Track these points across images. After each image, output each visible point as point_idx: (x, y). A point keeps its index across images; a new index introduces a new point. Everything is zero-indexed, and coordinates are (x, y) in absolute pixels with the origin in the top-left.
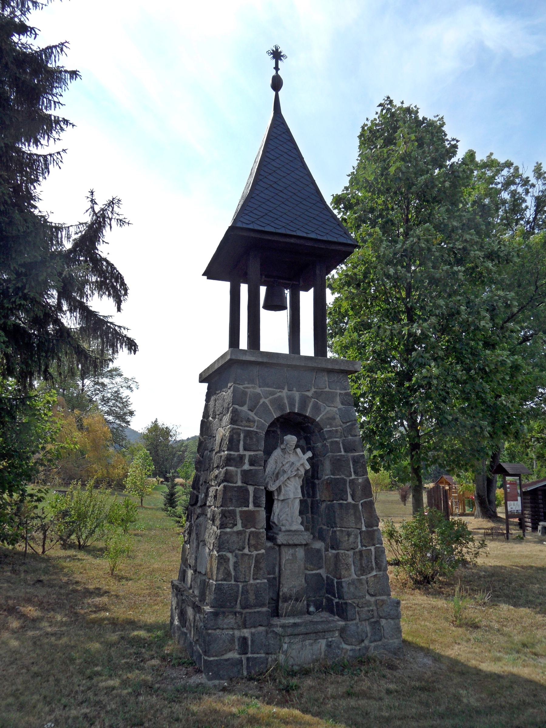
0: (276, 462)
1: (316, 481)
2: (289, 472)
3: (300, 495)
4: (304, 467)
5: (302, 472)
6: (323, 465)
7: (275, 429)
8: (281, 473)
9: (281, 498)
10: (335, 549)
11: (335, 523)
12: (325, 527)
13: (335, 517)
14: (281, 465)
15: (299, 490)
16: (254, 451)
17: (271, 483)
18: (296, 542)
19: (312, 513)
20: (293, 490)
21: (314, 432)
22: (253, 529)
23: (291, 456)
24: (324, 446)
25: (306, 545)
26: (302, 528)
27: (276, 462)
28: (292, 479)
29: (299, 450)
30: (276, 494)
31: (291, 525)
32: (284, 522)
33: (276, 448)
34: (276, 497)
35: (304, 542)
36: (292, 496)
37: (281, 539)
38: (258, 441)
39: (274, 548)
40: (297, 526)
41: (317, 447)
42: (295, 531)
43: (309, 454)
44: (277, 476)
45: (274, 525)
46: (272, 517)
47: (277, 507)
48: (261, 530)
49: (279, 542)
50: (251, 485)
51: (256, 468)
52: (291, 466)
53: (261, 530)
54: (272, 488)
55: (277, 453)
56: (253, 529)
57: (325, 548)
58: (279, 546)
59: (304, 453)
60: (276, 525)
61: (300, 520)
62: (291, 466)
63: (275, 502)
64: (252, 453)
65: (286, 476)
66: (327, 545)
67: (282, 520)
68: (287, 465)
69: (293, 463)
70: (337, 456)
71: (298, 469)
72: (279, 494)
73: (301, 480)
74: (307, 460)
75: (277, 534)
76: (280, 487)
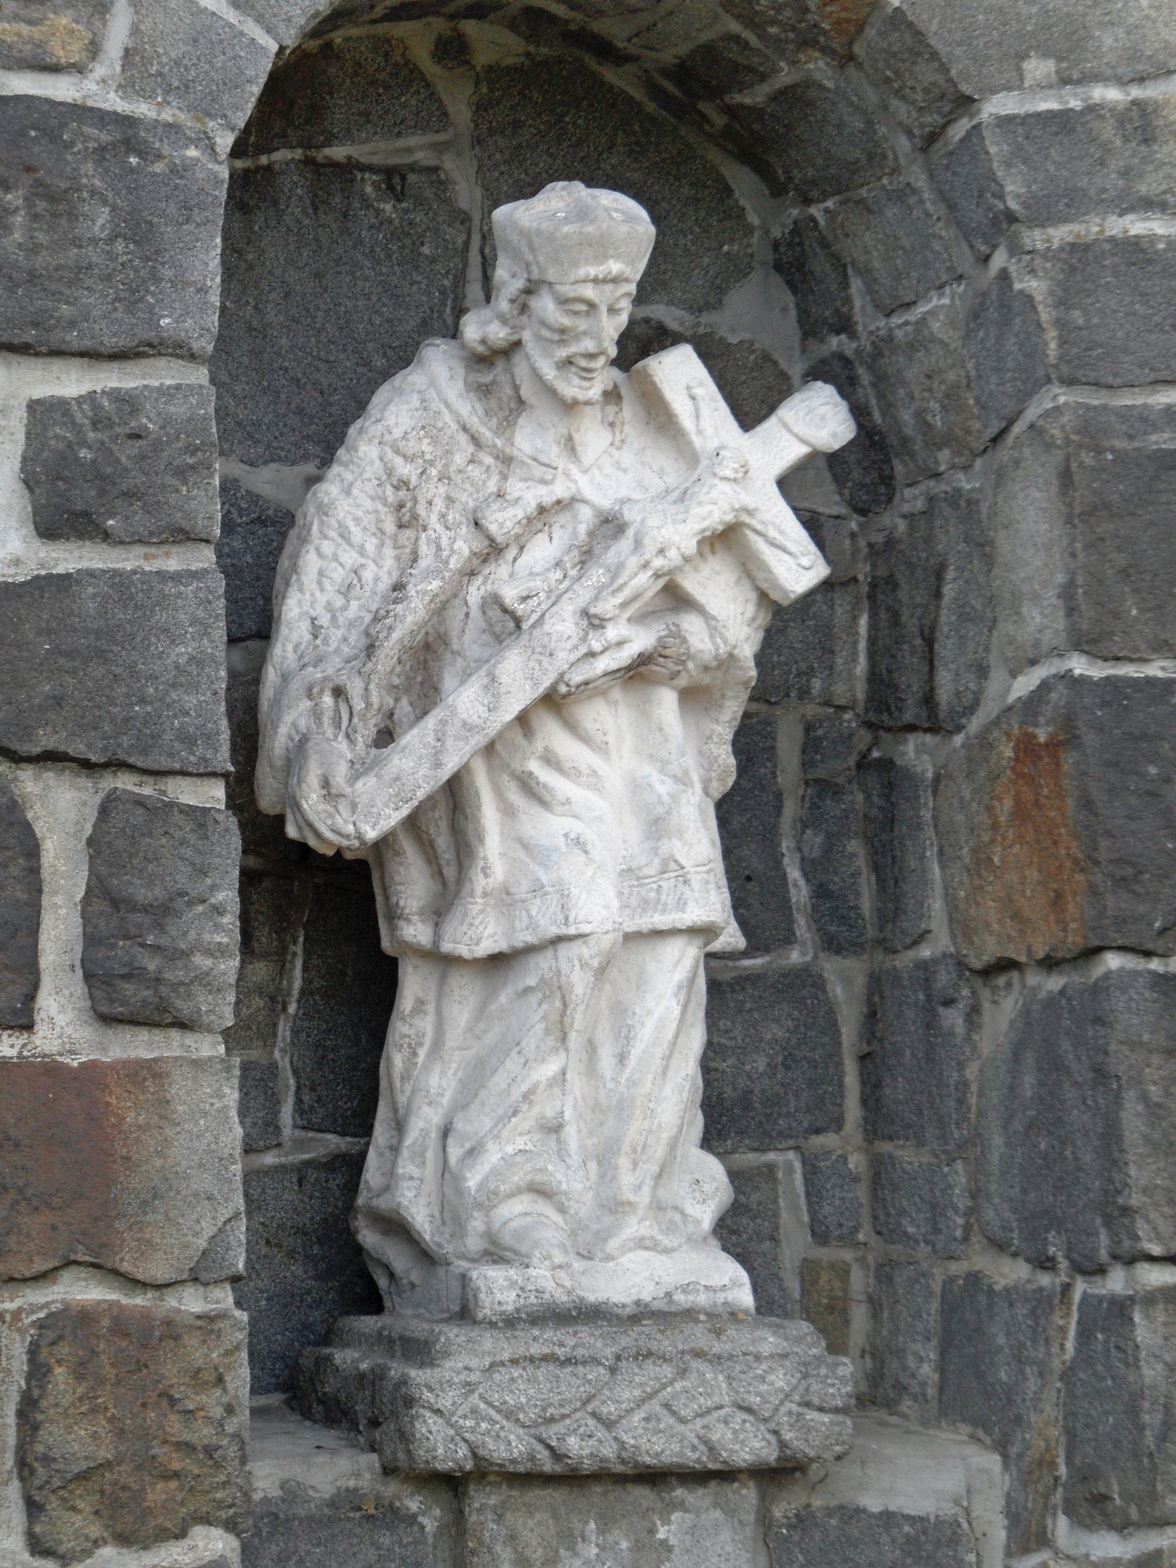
0: (407, 519)
1: (916, 754)
2: (563, 625)
3: (707, 901)
4: (750, 569)
5: (727, 623)
6: (983, 549)
7: (416, 147)
8: (469, 638)
9: (480, 931)
10: (1122, 1526)
11: (1118, 1216)
12: (1011, 1273)
13: (1111, 1139)
14: (463, 546)
15: (699, 844)
16: (93, 355)
17: (336, 754)
18: (662, 1446)
19: (878, 1120)
20: (609, 853)
21: (875, 157)
22: (84, 1291)
23: (594, 437)
24: (999, 307)
25: (778, 1474)
26: (728, 1281)
27: (407, 519)
28: (599, 716)
29: (680, 373)
30: (410, 885)
31: (589, 1247)
32: (514, 1212)
33: (403, 357)
34: (416, 932)
35: (749, 1446)
36: (598, 908)
37: (466, 1403)
38: (137, 229)
39: (391, 1516)
40: (664, 1246)
41: (920, 341)
42: (641, 1314)
43: (816, 420)
44: (424, 671)
45: (397, 1256)
46: (372, 1174)
47: (432, 1047)
48: (191, 1302)
49: (439, 1441)
50: (51, 758)
51: (127, 560)
52: (587, 556)
53: (191, 1302)
54: (350, 803)
55: (420, 409)
56: (84, 1291)
57: (1014, 1516)
58: (451, 1485)
59: (750, 411)
60: (427, 1257)
61: (705, 1186)
62: (587, 556)
63: (413, 985)
64: (70, 383)
65: (518, 679)
66: (1030, 1472)
67: (489, 1199)
68: (542, 551)
69: (611, 525)
70: (1145, 420)
71: (674, 597)
72: (445, 902)
73: (722, 727)
74: (789, 484)
75: (421, 1351)
76: (454, 794)
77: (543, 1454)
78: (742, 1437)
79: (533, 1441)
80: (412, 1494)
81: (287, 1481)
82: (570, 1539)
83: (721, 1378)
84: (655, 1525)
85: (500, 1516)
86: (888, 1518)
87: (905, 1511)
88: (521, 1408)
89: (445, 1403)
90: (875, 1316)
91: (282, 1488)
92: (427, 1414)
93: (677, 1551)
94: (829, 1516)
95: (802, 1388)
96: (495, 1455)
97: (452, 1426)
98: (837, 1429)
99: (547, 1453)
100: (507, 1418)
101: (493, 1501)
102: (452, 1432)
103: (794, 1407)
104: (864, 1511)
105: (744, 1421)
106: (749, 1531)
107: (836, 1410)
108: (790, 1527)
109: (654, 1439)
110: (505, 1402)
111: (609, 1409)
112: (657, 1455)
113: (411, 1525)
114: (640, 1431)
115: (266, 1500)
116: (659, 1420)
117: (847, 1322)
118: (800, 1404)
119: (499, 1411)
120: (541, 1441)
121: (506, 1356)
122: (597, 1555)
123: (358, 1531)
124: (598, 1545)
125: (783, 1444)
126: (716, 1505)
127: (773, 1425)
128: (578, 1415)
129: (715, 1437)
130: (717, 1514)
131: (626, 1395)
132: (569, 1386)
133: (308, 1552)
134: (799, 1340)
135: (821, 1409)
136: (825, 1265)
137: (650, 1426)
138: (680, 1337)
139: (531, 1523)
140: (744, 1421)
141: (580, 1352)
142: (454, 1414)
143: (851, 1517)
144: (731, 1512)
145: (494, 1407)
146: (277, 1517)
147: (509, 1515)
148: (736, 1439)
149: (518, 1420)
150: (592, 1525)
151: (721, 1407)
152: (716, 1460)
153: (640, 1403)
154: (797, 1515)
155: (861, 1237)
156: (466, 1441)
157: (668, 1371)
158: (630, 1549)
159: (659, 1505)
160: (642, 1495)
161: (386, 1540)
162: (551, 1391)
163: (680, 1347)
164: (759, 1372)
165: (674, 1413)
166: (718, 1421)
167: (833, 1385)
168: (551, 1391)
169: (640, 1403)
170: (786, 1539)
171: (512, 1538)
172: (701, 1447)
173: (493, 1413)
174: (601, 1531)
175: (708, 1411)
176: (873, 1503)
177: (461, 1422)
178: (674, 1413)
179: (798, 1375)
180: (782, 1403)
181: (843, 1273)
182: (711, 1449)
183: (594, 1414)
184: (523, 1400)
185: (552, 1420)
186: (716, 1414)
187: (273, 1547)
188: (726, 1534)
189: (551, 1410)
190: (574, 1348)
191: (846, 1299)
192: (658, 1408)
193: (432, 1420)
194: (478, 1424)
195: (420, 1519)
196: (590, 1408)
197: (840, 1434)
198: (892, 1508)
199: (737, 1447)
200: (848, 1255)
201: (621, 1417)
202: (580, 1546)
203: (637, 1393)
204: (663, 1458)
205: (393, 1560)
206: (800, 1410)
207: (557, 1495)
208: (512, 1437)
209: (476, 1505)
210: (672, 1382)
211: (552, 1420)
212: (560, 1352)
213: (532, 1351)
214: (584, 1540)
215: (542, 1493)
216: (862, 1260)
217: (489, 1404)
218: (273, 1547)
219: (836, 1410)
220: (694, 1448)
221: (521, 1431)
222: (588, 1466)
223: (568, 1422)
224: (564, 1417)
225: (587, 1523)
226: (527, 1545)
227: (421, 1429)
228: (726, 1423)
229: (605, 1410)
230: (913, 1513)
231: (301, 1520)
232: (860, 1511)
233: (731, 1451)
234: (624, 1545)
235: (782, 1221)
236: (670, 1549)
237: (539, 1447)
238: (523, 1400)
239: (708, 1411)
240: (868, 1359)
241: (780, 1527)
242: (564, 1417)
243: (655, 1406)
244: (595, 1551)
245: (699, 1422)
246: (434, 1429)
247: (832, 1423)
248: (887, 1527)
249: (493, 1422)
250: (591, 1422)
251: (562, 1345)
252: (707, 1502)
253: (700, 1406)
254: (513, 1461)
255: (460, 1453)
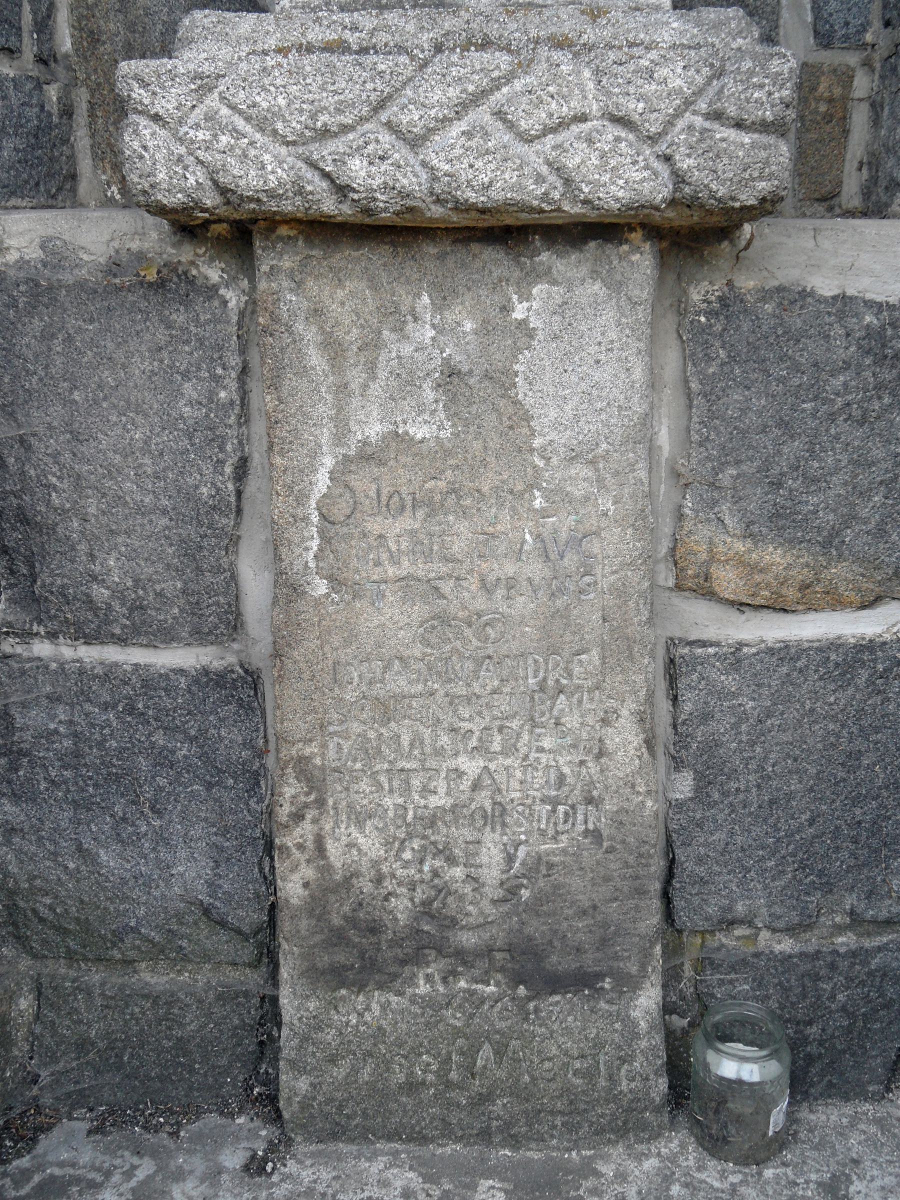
18: (493, 171)
25: (689, 234)
35: (623, 177)
77: (317, 185)
78: (613, 163)
79: (300, 164)
80: (212, 260)
81: (50, 239)
82: (398, 319)
83: (587, 73)
84: (509, 300)
85: (299, 284)
86: (844, 304)
87: (869, 296)
88: (278, 114)
89: (165, 105)
90: (876, 122)
91: (43, 247)
92: (143, 121)
93: (540, 335)
94: (763, 300)
95: (711, 92)
96: (242, 183)
97: (181, 140)
98: (763, 154)
99: (325, 184)
100: (262, 130)
101: (287, 263)
102: (182, 150)
103: (698, 121)
104: (812, 294)
105: (618, 139)
106: (642, 313)
107: (764, 127)
108: (709, 314)
109: (479, 164)
110: (254, 105)
111: (411, 118)
112: (487, 187)
113: (210, 298)
114: (458, 151)
115: (22, 264)
116: (486, 135)
117: (846, 132)
118: (707, 116)
119: (248, 119)
120: (313, 165)
121: (272, 43)
122: (433, 339)
123: (143, 304)
124: (433, 326)
125: (679, 178)
126: (595, 274)
127: (662, 148)
128: (368, 126)
129: (571, 162)
130: (597, 287)
131: (437, 96)
132: (353, 83)
133: (79, 330)
134: (717, 26)
135: (739, 125)
136: (825, 68)
137: (473, 144)
138: (537, 20)
139: (340, 294)
140: (618, 139)
141: (382, 38)
142: (181, 122)
143: (793, 302)
144: (615, 286)
145: (240, 113)
146: (37, 285)
147: (310, 283)
148: (602, 168)
149: (275, 132)
150: (426, 299)
151: (582, 118)
152: (575, 200)
153: (462, 108)
154: (721, 299)
155: (869, 37)
156: (200, 162)
157: (503, 60)
158: (476, 332)
159: (517, 273)
160: (493, 260)
161: (179, 318)
162: (323, 88)
163: (533, 33)
164: (645, 63)
165: (511, 126)
166: (578, 138)
167: (761, 86)
168: (323, 88)
169: (462, 108)
170: (704, 329)
171: (317, 313)
172: (552, 178)
173: (240, 123)
174: (440, 306)
175: (563, 124)
176: (826, 286)
177: (192, 133)
178: (511, 126)
179: (706, 71)
180: (678, 114)
181: (846, 78)
182: (567, 182)
183: (390, 126)
184: (282, 101)
185: (325, 134)
186: (575, 129)
187: (36, 321)
188: (608, 316)
189: (323, 118)
190: (372, 32)
191: (845, 99)
192: (487, 117)
193: (146, 127)
194: (215, 136)
195: (222, 291)
196: (384, 117)
197: (767, 163)
198: (850, 292)
199: (606, 178)
200: (853, 59)
201: (431, 131)
202: (410, 326)
203: (453, 92)
204: (492, 194)
205: (187, 342)
206: (707, 125)
207: (374, 257)
208: (267, 157)
209: (265, 268)
210: (509, 78)
211: (325, 134)
212: (352, 38)
213: (310, 36)
214: (416, 319)
215: (355, 254)
216: (867, 64)
217: (233, 108)
218: (36, 321)
219: (764, 127)
220: (540, 179)
221: (283, 150)
222: (386, 207)
223: (351, 136)
224: (345, 129)
225: (418, 296)
226: (337, 324)
227: (131, 143)
228: (590, 141)
229: (405, 119)
230: (880, 299)
231: (69, 289)
232: (805, 294)
233: (596, 184)
234: (468, 326)
235: (782, 22)
236: (531, 334)
237: (309, 174)
238: (282, 101)
239: (563, 124)
240: (865, 171)
241: (698, 314)
242: (345, 129)
243: (482, 115)
244: (431, 333)
245: (550, 140)
246: (150, 144)
247: (753, 145)
248: (841, 316)
249: (238, 134)
250: (386, 138)
251: (355, 28)
252: (584, 270)
253: (551, 115)
254: (272, 194)
255: (192, 180)
